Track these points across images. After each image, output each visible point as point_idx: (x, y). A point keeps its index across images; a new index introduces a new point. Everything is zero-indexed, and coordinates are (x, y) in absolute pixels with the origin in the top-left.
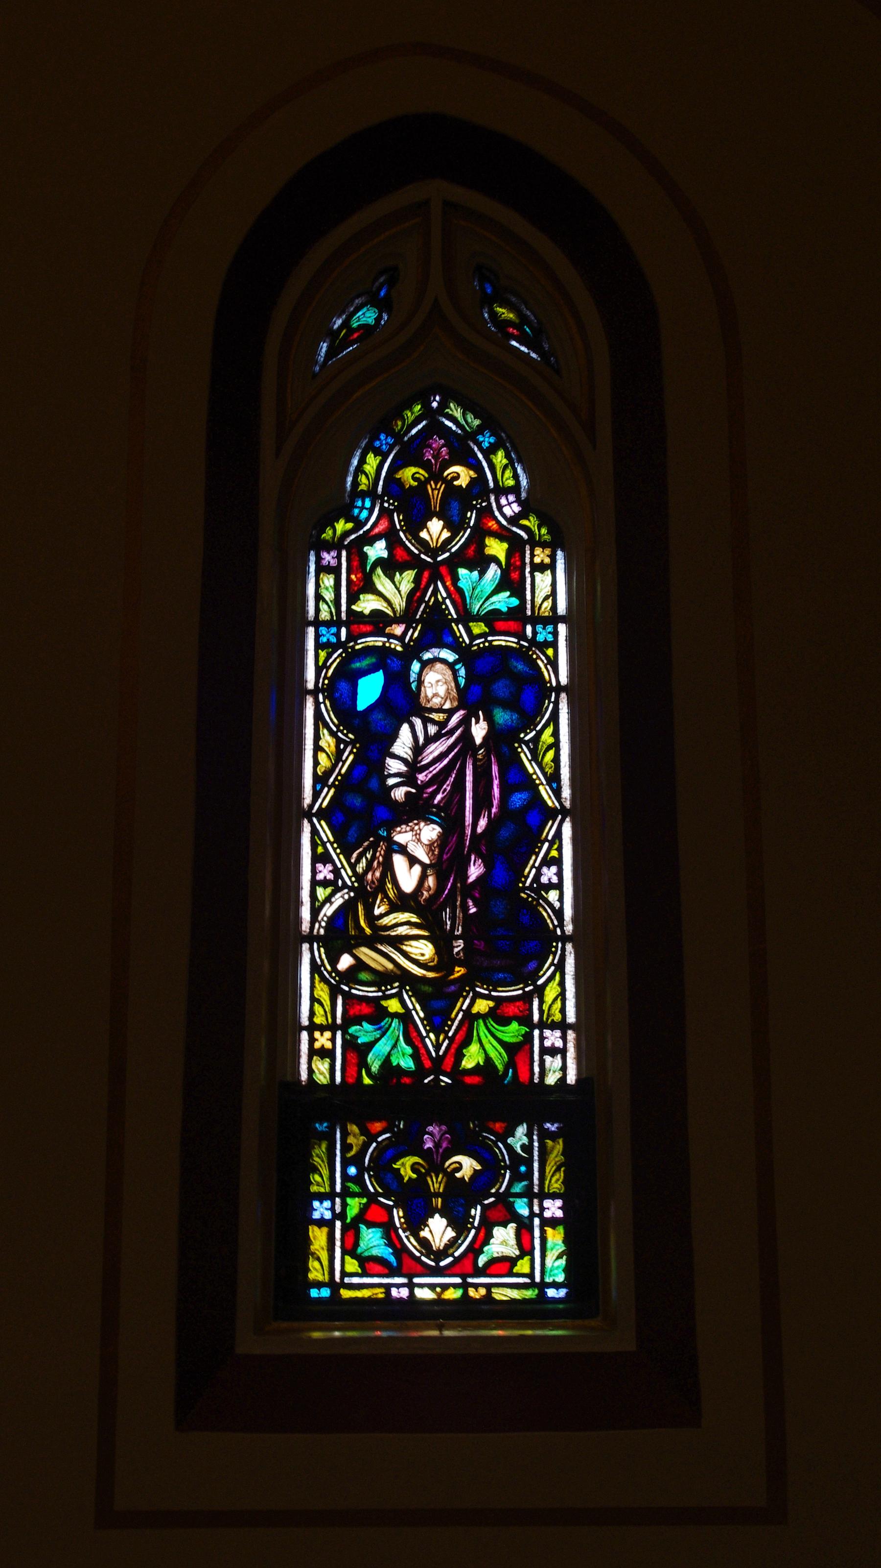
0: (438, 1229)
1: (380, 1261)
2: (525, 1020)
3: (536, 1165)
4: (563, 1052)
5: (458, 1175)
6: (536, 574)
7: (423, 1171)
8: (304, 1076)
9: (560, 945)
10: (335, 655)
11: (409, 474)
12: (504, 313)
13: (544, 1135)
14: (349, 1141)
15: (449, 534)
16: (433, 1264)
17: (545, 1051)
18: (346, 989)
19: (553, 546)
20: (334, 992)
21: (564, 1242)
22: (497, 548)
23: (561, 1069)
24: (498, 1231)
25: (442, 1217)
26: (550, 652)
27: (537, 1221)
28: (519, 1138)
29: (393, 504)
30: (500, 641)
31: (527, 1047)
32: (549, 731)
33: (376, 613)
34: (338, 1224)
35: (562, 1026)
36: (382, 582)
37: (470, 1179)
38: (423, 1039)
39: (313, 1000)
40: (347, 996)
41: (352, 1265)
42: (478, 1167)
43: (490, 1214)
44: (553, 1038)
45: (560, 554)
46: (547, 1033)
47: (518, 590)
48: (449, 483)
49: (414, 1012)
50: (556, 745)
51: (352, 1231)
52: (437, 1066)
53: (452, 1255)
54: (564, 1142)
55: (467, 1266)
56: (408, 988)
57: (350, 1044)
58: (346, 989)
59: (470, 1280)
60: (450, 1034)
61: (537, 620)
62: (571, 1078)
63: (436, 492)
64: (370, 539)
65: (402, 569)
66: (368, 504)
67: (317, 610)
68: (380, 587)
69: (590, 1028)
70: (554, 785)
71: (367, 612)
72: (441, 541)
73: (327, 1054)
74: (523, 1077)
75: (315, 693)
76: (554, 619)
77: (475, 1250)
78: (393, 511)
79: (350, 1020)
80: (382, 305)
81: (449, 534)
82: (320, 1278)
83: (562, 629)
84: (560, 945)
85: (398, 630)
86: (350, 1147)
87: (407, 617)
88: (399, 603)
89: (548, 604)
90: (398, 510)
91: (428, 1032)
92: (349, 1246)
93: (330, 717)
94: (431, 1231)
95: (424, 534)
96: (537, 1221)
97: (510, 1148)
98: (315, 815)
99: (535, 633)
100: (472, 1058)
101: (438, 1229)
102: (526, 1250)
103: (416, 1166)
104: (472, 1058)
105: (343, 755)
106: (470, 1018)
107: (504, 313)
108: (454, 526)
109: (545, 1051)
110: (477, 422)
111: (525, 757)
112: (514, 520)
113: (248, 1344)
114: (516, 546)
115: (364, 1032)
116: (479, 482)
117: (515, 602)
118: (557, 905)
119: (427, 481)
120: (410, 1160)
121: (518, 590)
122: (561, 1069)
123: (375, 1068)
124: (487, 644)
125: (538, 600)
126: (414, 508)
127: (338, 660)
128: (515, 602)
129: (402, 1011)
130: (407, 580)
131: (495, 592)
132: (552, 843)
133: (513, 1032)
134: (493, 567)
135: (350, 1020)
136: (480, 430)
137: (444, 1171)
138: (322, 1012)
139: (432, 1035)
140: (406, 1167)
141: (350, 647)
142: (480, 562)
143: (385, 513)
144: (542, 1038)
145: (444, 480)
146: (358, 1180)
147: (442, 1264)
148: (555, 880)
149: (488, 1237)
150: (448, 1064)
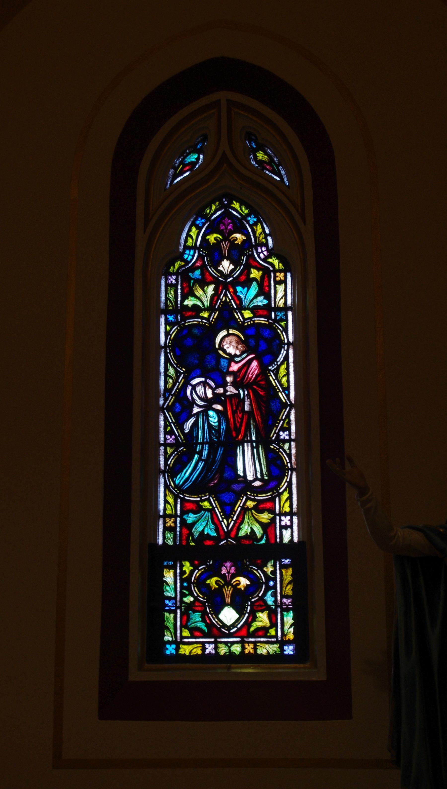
0: (228, 615)
1: (199, 629)
2: (272, 511)
3: (278, 579)
4: (291, 527)
5: (236, 242)
6: (277, 286)
7: (221, 584)
8: (160, 541)
9: (290, 473)
10: (174, 329)
11: (212, 238)
12: (261, 156)
13: (283, 567)
14: (184, 569)
15: (233, 267)
16: (227, 632)
17: (283, 527)
18: (182, 496)
19: (285, 271)
20: (176, 497)
21: (293, 619)
22: (255, 274)
23: (290, 533)
24: (259, 615)
25: (227, 260)
26: (283, 324)
27: (279, 610)
28: (269, 569)
29: (205, 253)
30: (258, 320)
31: (273, 525)
32: (284, 366)
33: (194, 306)
34: (179, 611)
35: (291, 514)
36: (199, 292)
37: (241, 243)
38: (220, 522)
39: (166, 502)
40: (183, 501)
41: (186, 633)
42: (248, 583)
43: (255, 608)
44: (286, 520)
45: (289, 275)
46: (283, 518)
47: (268, 296)
48: (235, 587)
49: (216, 509)
50: (287, 377)
51: (186, 617)
52: (227, 535)
53: (233, 277)
54: (292, 569)
55: (244, 633)
56: (240, 323)
57: (183, 522)
58: (182, 496)
59: (246, 640)
60: (219, 301)
61: (277, 309)
62: (296, 540)
63: (225, 246)
64: (193, 269)
65: (208, 284)
66: (192, 252)
67: (165, 509)
68: (197, 294)
69: (304, 512)
70: (287, 392)
71: (190, 306)
72: (229, 270)
73: (172, 529)
74: (273, 541)
75: (166, 346)
76: (285, 309)
77: (248, 624)
78: (204, 256)
79: (184, 512)
80: (199, 152)
81: (233, 267)
82: (170, 639)
83: (290, 314)
84: (290, 473)
85: (206, 315)
86: (185, 572)
87: (211, 309)
88: (207, 303)
89: (283, 301)
90: (207, 255)
91: (223, 519)
92: (184, 623)
93: (173, 360)
94: (222, 266)
95: (220, 268)
96: (279, 610)
97: (265, 573)
98: (166, 409)
99: (276, 316)
100: (245, 530)
101: (228, 615)
102: (273, 624)
103: (218, 582)
104: (245, 530)
105: (179, 379)
106: (245, 510)
107: (261, 156)
108: (236, 262)
109: (283, 527)
110: (246, 212)
111: (272, 378)
112: (264, 260)
113: (135, 675)
114: (266, 273)
115: (191, 518)
116: (247, 242)
117: (266, 302)
118: (286, 385)
119: (221, 241)
120: (214, 579)
121: (268, 296)
122: (290, 533)
123: (196, 535)
124: (252, 322)
125: (277, 300)
126: (213, 254)
127: (176, 330)
128: (266, 302)
129: (243, 312)
130: (210, 290)
131: (256, 296)
132: (284, 420)
133: (265, 517)
134: (254, 283)
135: (184, 512)
136: (248, 215)
137: (232, 585)
138: (170, 508)
139: (225, 521)
140: (212, 582)
141: (183, 324)
142: (247, 283)
143: (200, 257)
144: (280, 521)
145: (229, 241)
146: (189, 588)
147: (232, 631)
148: (289, 523)
149: (254, 618)
150: (233, 534)
